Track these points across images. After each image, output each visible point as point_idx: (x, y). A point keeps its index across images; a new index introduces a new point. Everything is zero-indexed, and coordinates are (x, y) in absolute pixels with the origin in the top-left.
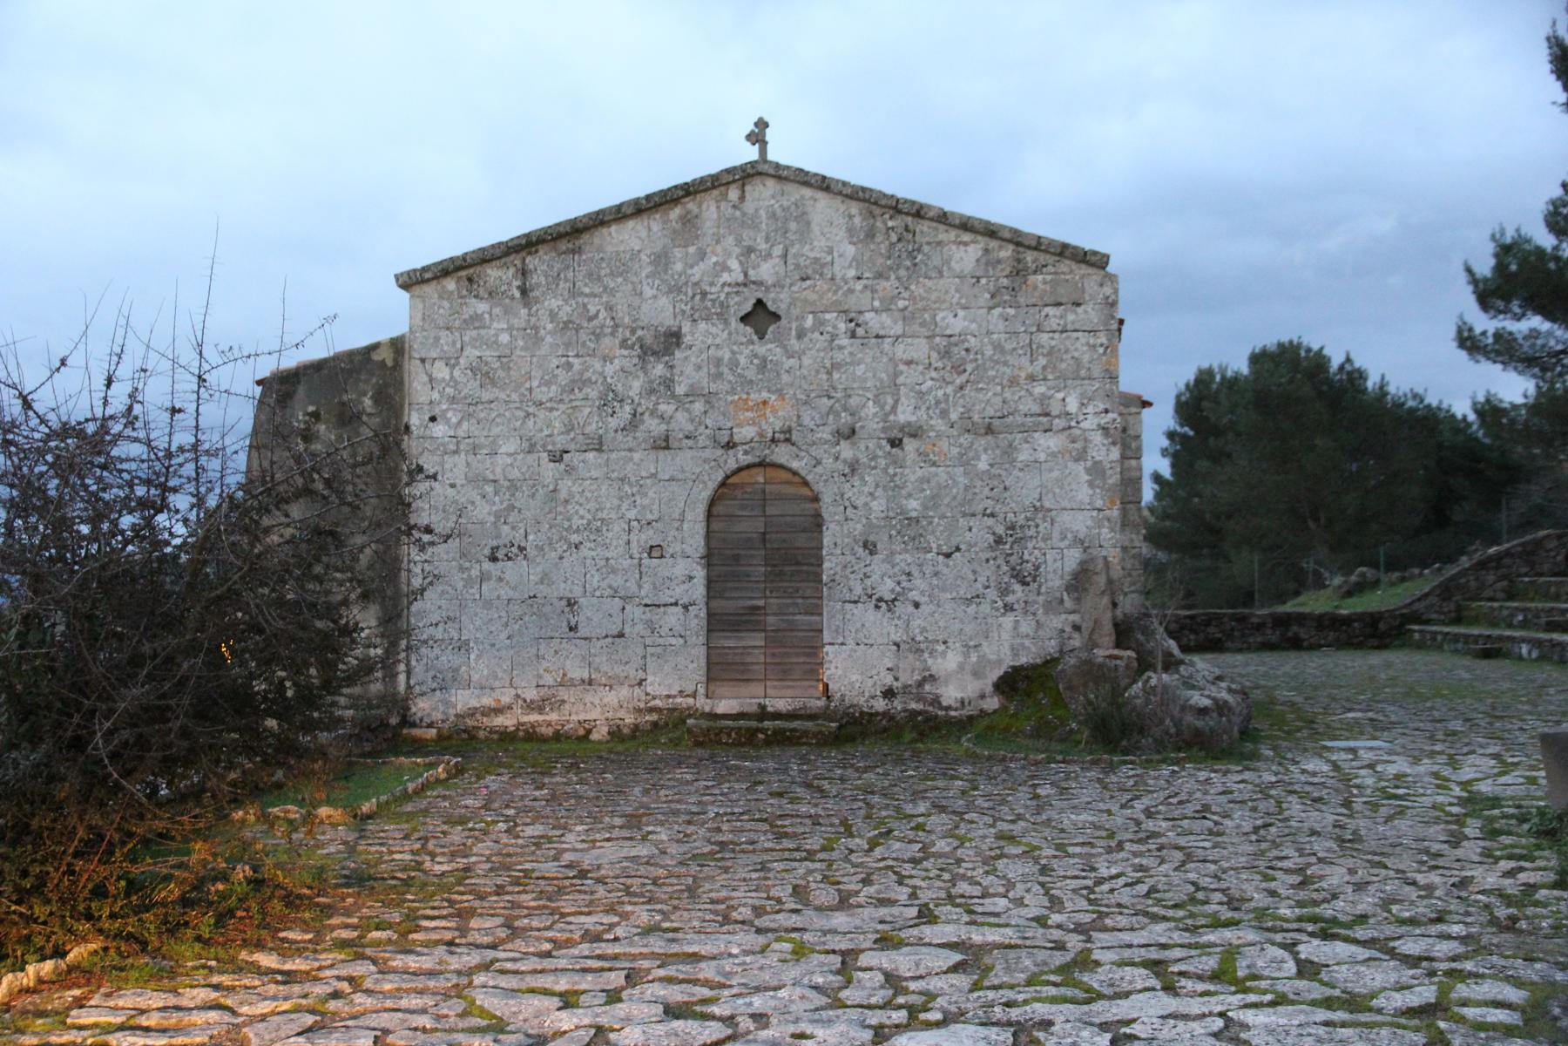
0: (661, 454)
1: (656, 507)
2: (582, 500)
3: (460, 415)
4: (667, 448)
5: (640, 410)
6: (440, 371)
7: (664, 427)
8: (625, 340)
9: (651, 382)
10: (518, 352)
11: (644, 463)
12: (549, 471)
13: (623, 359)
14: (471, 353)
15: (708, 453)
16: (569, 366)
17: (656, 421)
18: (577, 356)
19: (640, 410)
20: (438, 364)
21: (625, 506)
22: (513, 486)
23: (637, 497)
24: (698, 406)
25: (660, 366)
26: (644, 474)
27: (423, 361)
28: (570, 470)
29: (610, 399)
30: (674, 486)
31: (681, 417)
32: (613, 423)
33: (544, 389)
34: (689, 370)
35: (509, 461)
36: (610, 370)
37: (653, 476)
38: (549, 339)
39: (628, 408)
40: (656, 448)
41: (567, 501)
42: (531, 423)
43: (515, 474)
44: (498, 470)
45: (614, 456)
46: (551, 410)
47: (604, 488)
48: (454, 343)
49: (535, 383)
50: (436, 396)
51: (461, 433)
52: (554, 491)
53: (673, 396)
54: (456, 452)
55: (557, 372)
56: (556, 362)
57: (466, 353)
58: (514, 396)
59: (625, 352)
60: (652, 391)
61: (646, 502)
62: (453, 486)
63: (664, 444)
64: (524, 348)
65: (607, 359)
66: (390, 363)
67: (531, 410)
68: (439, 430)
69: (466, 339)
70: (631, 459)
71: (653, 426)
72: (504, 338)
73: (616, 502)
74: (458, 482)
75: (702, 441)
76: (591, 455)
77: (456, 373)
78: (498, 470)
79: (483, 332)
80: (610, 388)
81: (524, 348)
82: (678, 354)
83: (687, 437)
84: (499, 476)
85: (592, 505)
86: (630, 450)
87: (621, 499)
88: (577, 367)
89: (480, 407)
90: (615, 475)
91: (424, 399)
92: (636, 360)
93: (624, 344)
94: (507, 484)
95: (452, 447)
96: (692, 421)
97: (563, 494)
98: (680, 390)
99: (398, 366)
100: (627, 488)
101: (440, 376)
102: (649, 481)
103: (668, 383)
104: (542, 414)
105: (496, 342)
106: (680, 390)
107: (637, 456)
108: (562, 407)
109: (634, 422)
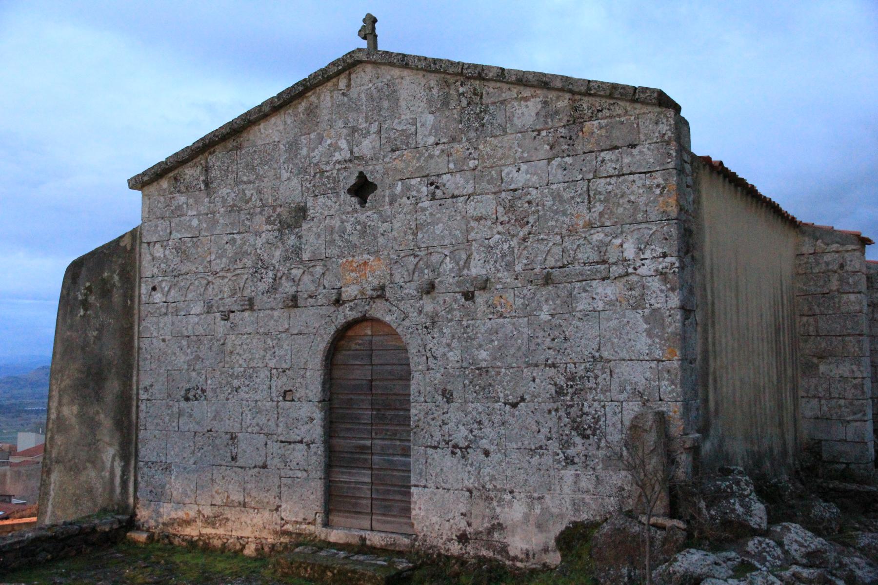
0: (293, 311)
1: (288, 357)
2: (241, 352)
3: (169, 284)
4: (296, 306)
5: (279, 275)
6: (158, 251)
7: (294, 288)
8: (269, 217)
9: (287, 251)
10: (203, 233)
11: (279, 320)
12: (221, 327)
13: (268, 233)
14: (176, 235)
15: (324, 311)
16: (234, 240)
17: (291, 283)
18: (239, 233)
19: (279, 275)
20: (158, 246)
21: (268, 356)
22: (199, 339)
23: (276, 349)
24: (319, 269)
25: (293, 237)
26: (281, 329)
27: (149, 243)
28: (234, 326)
29: (260, 266)
30: (300, 339)
31: (306, 278)
32: (262, 286)
33: (218, 261)
34: (312, 239)
35: (196, 319)
36: (259, 242)
37: (287, 330)
38: (221, 221)
39: (271, 274)
40: (287, 307)
41: (231, 352)
42: (210, 289)
43: (200, 330)
44: (190, 327)
45: (261, 315)
46: (223, 277)
47: (255, 341)
48: (166, 229)
49: (213, 257)
50: (156, 270)
51: (170, 299)
52: (223, 344)
53: (301, 262)
54: (166, 314)
55: (227, 246)
56: (226, 239)
57: (172, 236)
58: (201, 269)
59: (269, 227)
60: (287, 259)
61: (282, 353)
62: (164, 340)
63: (294, 302)
64: (207, 230)
65: (258, 234)
66: (129, 248)
67: (210, 279)
68: (158, 297)
69: (173, 225)
70: (272, 317)
71: (288, 288)
72: (195, 222)
73: (262, 353)
74: (167, 338)
75: (321, 300)
76: (247, 314)
77: (167, 252)
78: (190, 327)
79: (182, 218)
80: (259, 258)
81: (207, 230)
82: (305, 226)
83: (311, 297)
84: (190, 333)
85: (247, 356)
86: (272, 309)
87: (265, 350)
88: (239, 242)
89: (181, 278)
90: (261, 330)
91: (149, 274)
92: (276, 233)
93: (268, 221)
94: (195, 338)
95: (164, 310)
96: (313, 282)
97: (229, 347)
98: (306, 256)
99: (133, 248)
100: (269, 341)
101: (158, 255)
102: (284, 335)
103: (298, 251)
104: (218, 282)
105: (190, 226)
106: (306, 256)
107: (276, 314)
108: (229, 275)
109: (274, 288)
